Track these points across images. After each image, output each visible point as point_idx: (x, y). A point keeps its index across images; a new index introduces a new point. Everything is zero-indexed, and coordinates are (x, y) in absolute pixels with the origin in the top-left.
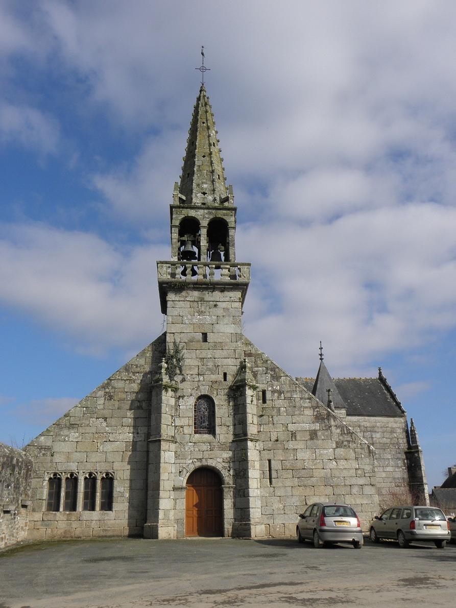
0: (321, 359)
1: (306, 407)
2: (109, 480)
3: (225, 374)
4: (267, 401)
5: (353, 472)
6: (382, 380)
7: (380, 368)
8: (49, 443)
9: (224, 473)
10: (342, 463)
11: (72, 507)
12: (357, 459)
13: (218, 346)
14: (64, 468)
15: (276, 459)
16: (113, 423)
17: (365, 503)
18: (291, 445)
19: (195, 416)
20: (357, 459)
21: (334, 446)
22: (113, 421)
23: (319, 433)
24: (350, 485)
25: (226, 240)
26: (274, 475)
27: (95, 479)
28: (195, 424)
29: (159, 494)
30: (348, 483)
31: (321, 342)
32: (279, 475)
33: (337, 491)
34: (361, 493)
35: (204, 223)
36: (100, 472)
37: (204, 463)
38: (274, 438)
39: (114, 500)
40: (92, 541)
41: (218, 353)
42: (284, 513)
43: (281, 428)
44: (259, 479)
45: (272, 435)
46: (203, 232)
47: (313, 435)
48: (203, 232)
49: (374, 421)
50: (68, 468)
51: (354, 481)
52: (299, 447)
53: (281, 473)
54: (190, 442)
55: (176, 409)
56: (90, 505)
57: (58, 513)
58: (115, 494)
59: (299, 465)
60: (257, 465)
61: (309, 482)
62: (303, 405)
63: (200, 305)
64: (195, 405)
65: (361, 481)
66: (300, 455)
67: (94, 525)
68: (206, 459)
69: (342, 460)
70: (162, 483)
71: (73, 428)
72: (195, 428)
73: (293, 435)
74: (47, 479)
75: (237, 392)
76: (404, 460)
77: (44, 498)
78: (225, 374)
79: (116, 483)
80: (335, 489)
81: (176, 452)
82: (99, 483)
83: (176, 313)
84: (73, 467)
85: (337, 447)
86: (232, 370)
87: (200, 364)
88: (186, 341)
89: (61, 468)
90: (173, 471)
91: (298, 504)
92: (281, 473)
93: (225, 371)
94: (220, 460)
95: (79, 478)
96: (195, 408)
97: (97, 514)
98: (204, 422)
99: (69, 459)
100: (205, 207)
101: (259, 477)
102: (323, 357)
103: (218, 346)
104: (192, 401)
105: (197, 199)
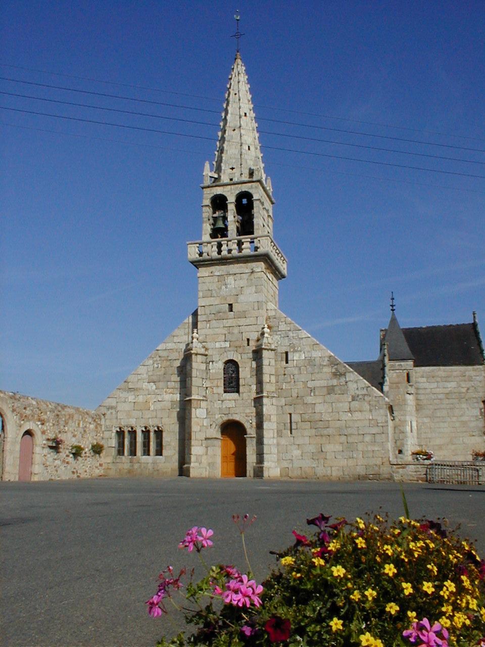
0: (393, 310)
1: (325, 366)
2: (159, 433)
3: (248, 340)
4: (289, 362)
5: (367, 423)
6: (474, 325)
7: (474, 312)
8: (114, 404)
9: (247, 426)
10: (357, 415)
11: (133, 452)
12: (371, 411)
13: (243, 315)
14: (126, 424)
15: (295, 412)
16: (160, 387)
17: (376, 449)
18: (309, 399)
19: (224, 378)
20: (371, 411)
21: (350, 399)
22: (161, 384)
23: (336, 389)
24: (363, 434)
25: (251, 212)
26: (294, 426)
27: (149, 431)
28: (224, 384)
29: (190, 443)
30: (361, 432)
31: (392, 293)
32: (298, 426)
33: (351, 440)
34: (373, 441)
35: (231, 199)
36: (153, 426)
37: (231, 418)
38: (295, 395)
39: (164, 448)
40: (3, 460)
41: (242, 321)
42: (302, 459)
43: (301, 385)
44: (276, 431)
45: (293, 392)
46: (231, 207)
47: (331, 390)
48: (231, 207)
49: (450, 370)
50: (129, 424)
51: (367, 430)
52: (318, 401)
53: (300, 424)
54: (219, 400)
55: (207, 373)
56: (147, 452)
57: (123, 457)
58: (164, 444)
59: (317, 417)
60: (274, 418)
61: (325, 432)
62: (322, 363)
63: (226, 278)
64: (224, 368)
65: (374, 431)
66: (318, 408)
67: (150, 466)
68: (232, 414)
69: (357, 413)
70: (193, 434)
71: (131, 391)
72: (225, 388)
73: (312, 390)
74: (115, 431)
75: (257, 354)
76: (481, 409)
77: (114, 446)
78: (248, 340)
79: (164, 434)
80: (349, 438)
81: (207, 409)
82: (152, 435)
83: (205, 288)
84: (132, 422)
85: (353, 400)
86: (254, 336)
87: (226, 332)
88: (215, 313)
89: (123, 423)
90: (205, 424)
91: (315, 451)
92: (300, 424)
93: (248, 337)
94: (245, 416)
95: (137, 431)
96: (224, 371)
97: (151, 458)
98: (232, 383)
99: (129, 415)
100: (232, 183)
101: (276, 427)
102: (394, 308)
103: (243, 315)
104: (220, 366)
105: (225, 179)
